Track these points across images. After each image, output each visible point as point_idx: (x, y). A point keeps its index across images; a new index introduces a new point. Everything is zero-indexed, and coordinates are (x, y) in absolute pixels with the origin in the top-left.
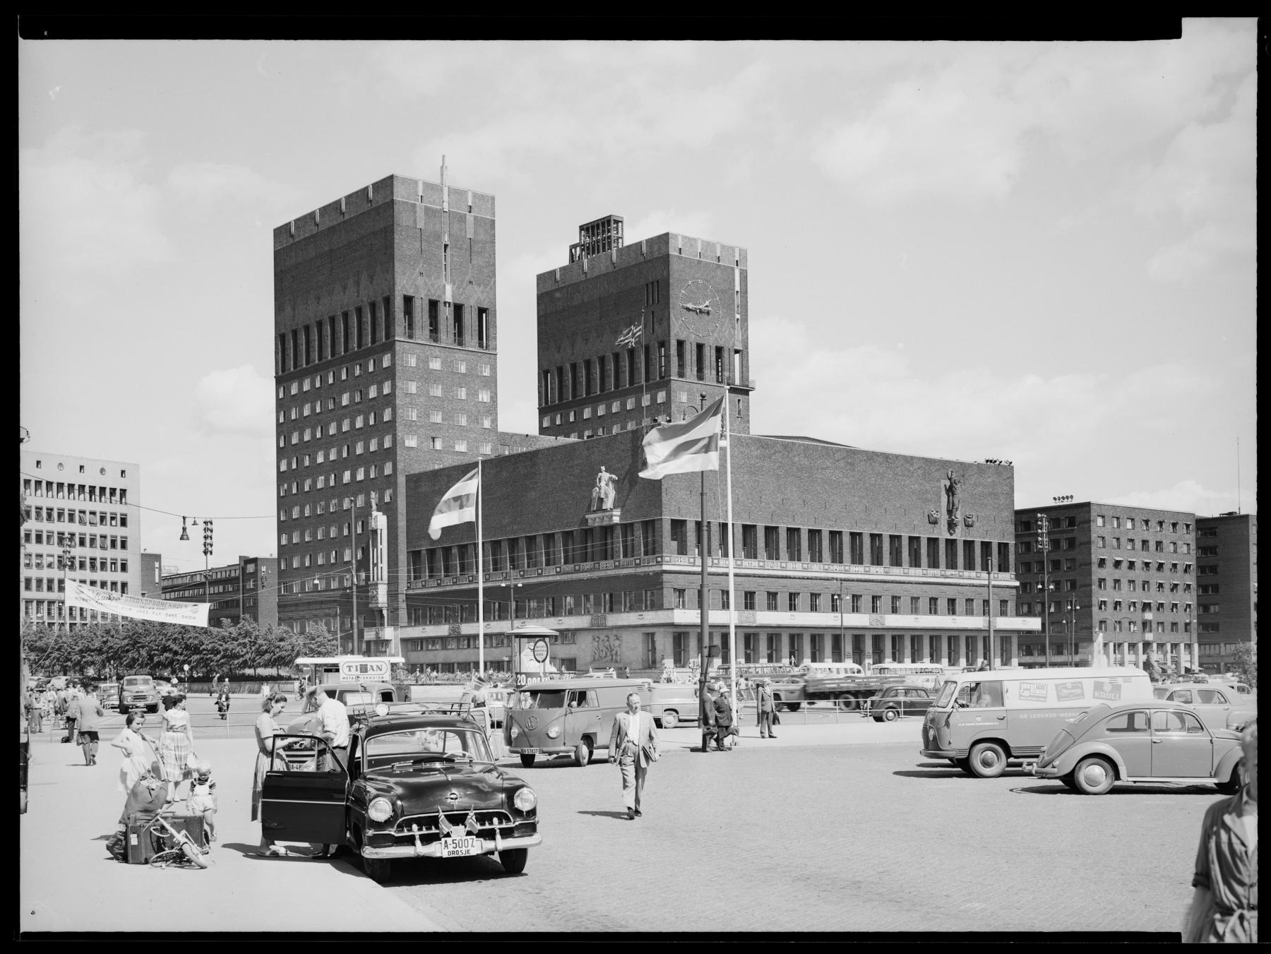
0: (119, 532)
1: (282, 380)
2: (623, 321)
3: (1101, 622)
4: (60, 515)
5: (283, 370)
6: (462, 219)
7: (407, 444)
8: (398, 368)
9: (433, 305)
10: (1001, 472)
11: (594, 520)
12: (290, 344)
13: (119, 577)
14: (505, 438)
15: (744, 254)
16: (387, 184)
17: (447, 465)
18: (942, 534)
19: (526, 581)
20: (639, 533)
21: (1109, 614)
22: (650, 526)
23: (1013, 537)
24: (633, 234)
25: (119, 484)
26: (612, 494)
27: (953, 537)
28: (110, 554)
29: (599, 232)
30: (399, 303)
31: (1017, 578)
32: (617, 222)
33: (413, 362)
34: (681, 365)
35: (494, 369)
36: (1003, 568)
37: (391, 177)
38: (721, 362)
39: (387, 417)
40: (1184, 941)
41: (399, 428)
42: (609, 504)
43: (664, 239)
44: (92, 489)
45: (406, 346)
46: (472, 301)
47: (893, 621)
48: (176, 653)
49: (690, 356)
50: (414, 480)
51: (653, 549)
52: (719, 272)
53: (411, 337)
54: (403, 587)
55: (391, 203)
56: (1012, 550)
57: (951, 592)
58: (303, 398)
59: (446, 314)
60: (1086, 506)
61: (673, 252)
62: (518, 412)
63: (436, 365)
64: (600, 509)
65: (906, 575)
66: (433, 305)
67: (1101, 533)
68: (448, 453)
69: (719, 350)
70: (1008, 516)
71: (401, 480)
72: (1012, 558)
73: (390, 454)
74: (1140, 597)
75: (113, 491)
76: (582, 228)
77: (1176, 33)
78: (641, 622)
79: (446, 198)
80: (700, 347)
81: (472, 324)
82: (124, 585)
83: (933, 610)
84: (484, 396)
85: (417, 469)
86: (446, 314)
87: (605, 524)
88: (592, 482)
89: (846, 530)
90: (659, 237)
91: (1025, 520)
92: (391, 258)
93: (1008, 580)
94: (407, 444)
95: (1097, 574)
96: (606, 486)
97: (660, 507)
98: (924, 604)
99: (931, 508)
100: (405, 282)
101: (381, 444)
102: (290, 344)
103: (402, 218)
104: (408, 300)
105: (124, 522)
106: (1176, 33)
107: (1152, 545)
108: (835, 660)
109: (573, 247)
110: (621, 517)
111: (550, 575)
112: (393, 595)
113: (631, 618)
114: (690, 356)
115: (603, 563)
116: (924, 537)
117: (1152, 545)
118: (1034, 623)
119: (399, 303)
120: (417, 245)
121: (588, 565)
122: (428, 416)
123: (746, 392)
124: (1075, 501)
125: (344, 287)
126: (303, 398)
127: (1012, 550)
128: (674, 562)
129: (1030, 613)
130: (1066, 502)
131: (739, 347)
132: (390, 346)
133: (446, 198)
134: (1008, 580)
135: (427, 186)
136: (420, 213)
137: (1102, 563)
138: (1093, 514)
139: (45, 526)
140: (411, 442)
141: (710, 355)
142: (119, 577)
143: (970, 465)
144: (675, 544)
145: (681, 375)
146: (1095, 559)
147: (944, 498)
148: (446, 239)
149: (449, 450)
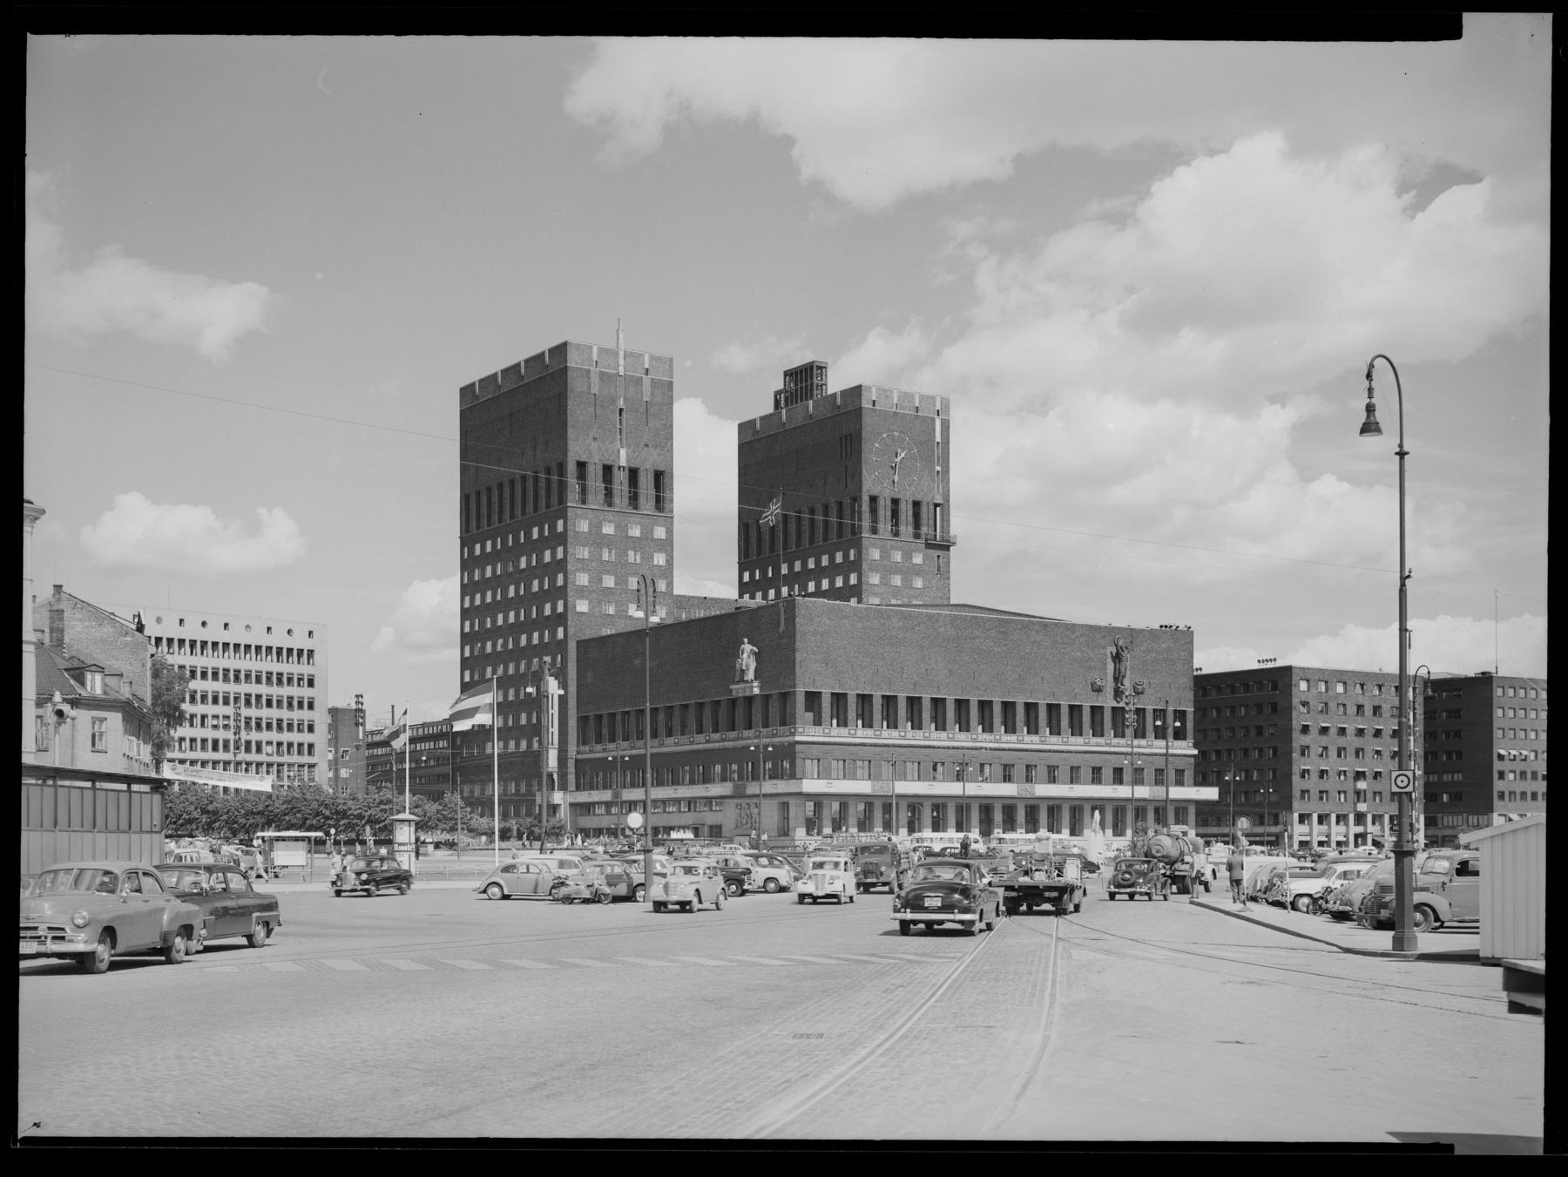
0: (306, 692)
1: (466, 542)
3: (1303, 792)
4: (248, 676)
5: (467, 531)
6: (639, 381)
7: (579, 609)
8: (570, 533)
9: (608, 470)
10: (1181, 639)
11: (737, 690)
12: (473, 506)
13: (306, 738)
14: (683, 602)
15: (946, 404)
16: (560, 350)
17: (620, 630)
18: (1108, 702)
19: (634, 752)
20: (633, 719)
21: (1313, 784)
22: (786, 697)
23: (1191, 704)
24: (836, 383)
25: (306, 645)
26: (753, 666)
28: (296, 715)
29: (803, 379)
31: (1195, 746)
33: (584, 526)
34: (875, 520)
35: (670, 532)
37: (565, 345)
38: (925, 523)
39: (560, 582)
40: (1457, 1152)
41: (570, 594)
42: (750, 675)
44: (280, 650)
45: (579, 512)
46: (647, 466)
47: (1044, 790)
48: (327, 818)
49: (884, 511)
50: (583, 645)
51: (787, 720)
52: (917, 423)
53: (584, 502)
54: (572, 750)
55: (565, 370)
57: (1096, 761)
58: (486, 558)
59: (621, 478)
61: (866, 404)
62: (707, 574)
63: (608, 529)
64: (742, 680)
65: (1066, 744)
66: (608, 470)
67: (1304, 698)
70: (1186, 682)
71: (572, 646)
73: (561, 619)
74: (1351, 764)
75: (300, 652)
77: (1455, 33)
79: (621, 362)
80: (895, 502)
81: (651, 487)
82: (311, 746)
83: (1074, 779)
84: (660, 559)
85: (589, 634)
86: (621, 478)
88: (736, 653)
89: (997, 700)
90: (853, 389)
91: (1207, 685)
92: (564, 425)
93: (1185, 748)
94: (579, 609)
95: (1299, 740)
96: (747, 658)
98: (1086, 773)
99: (1096, 677)
100: (577, 449)
101: (554, 609)
102: (473, 506)
103: (575, 385)
104: (581, 466)
105: (311, 683)
106: (1455, 33)
107: (1368, 710)
108: (1051, 830)
109: (777, 393)
110: (761, 688)
111: (700, 743)
112: (562, 760)
113: (769, 787)
114: (884, 511)
115: (746, 733)
116: (1087, 705)
117: (1368, 710)
118: (1211, 793)
119: (571, 468)
120: (591, 410)
121: (733, 734)
122: (600, 580)
123: (947, 548)
124: (1279, 664)
126: (486, 558)
128: (807, 733)
130: (1270, 665)
131: (939, 500)
132: (563, 514)
133: (621, 362)
134: (1186, 748)
136: (595, 379)
137: (1305, 729)
138: (1295, 678)
139: (199, 709)
140: (582, 606)
141: (906, 511)
142: (306, 738)
143: (1141, 631)
144: (810, 715)
145: (874, 531)
146: (1296, 724)
147: (1110, 666)
148: (621, 403)
149: (622, 614)
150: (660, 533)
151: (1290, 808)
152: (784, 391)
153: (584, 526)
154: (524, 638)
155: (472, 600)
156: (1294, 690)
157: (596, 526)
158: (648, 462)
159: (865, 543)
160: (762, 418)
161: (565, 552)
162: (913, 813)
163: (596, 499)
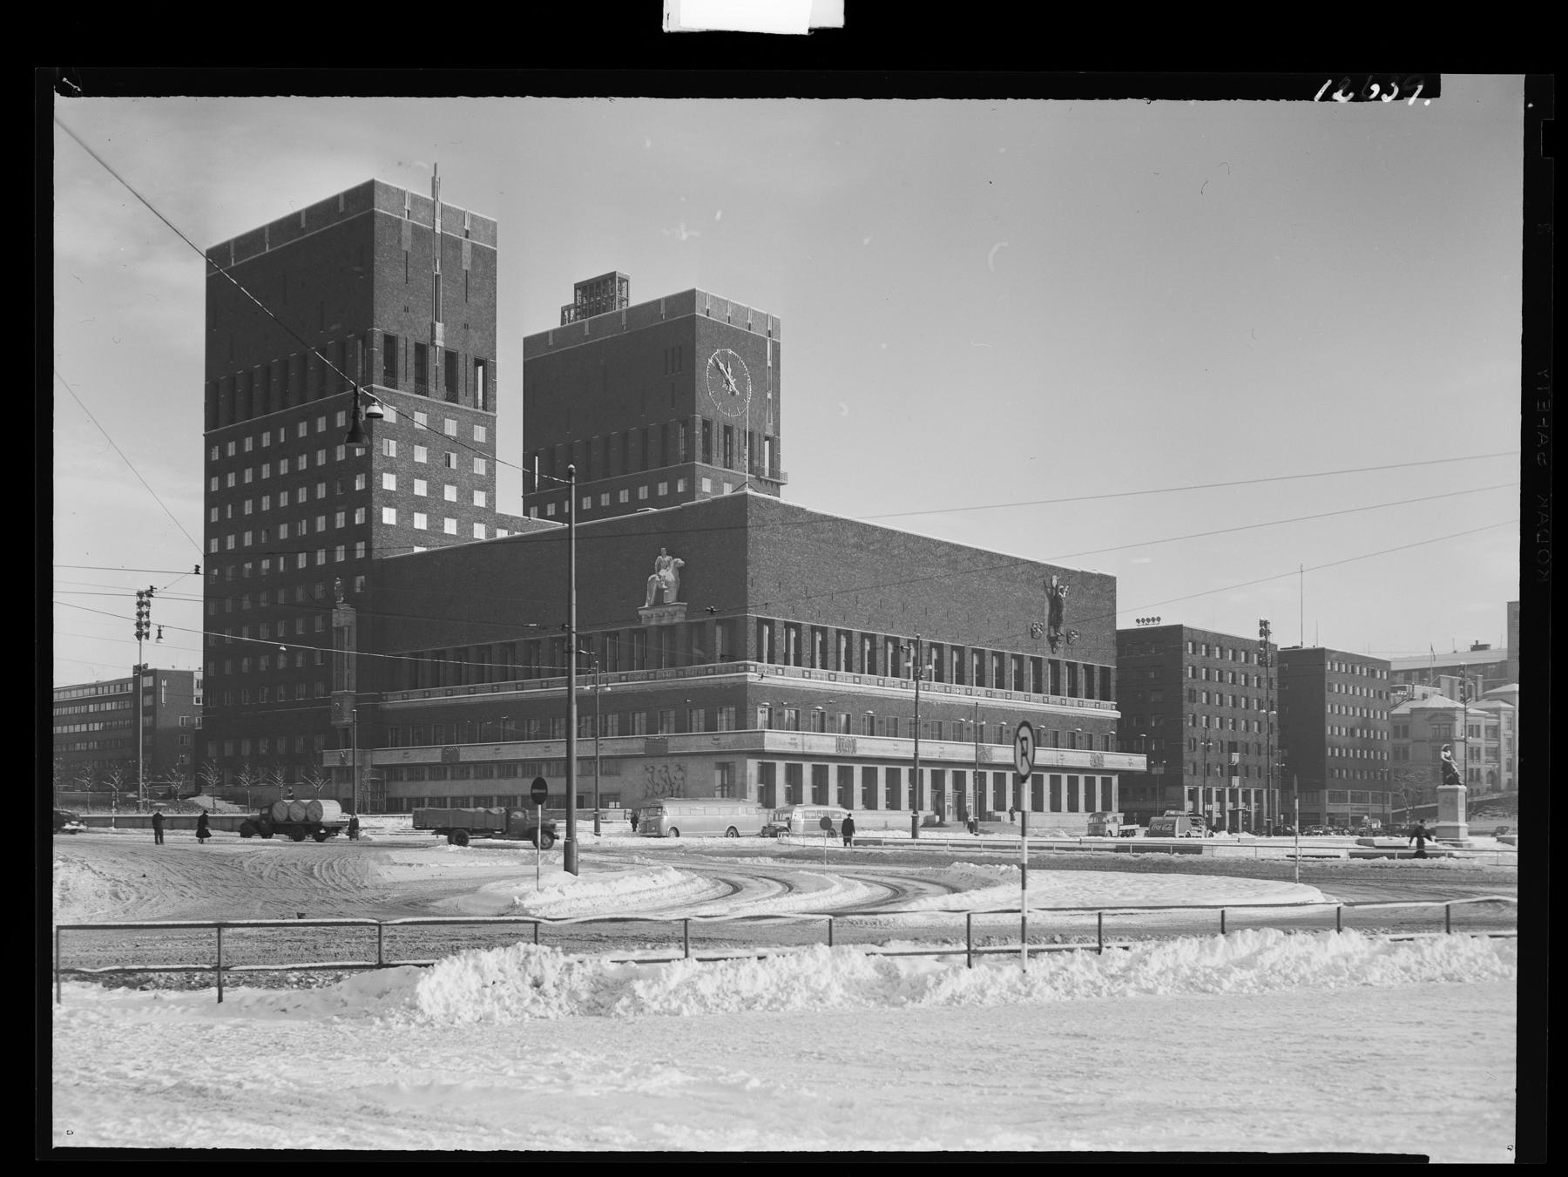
6: (457, 245)
9: (422, 351)
10: (1104, 586)
22: (734, 629)
24: (639, 295)
30: (378, 341)
32: (622, 280)
36: (1105, 697)
43: (690, 296)
56: (1113, 676)
60: (1178, 630)
68: (435, 535)
76: (578, 287)
81: (462, 376)
84: (480, 467)
87: (665, 622)
91: (1127, 639)
93: (1108, 711)
97: (745, 599)
100: (385, 322)
101: (350, 519)
109: (568, 308)
118: (1138, 762)
119: (378, 341)
120: (402, 271)
124: (1162, 624)
125: (302, 331)
127: (1113, 676)
130: (1151, 625)
131: (770, 433)
135: (416, 200)
136: (407, 233)
140: (389, 516)
145: (708, 460)
150: (480, 434)
151: (1180, 783)
152: (575, 306)
153: (390, 415)
155: (222, 544)
158: (468, 350)
159: (698, 472)
163: (406, 390)
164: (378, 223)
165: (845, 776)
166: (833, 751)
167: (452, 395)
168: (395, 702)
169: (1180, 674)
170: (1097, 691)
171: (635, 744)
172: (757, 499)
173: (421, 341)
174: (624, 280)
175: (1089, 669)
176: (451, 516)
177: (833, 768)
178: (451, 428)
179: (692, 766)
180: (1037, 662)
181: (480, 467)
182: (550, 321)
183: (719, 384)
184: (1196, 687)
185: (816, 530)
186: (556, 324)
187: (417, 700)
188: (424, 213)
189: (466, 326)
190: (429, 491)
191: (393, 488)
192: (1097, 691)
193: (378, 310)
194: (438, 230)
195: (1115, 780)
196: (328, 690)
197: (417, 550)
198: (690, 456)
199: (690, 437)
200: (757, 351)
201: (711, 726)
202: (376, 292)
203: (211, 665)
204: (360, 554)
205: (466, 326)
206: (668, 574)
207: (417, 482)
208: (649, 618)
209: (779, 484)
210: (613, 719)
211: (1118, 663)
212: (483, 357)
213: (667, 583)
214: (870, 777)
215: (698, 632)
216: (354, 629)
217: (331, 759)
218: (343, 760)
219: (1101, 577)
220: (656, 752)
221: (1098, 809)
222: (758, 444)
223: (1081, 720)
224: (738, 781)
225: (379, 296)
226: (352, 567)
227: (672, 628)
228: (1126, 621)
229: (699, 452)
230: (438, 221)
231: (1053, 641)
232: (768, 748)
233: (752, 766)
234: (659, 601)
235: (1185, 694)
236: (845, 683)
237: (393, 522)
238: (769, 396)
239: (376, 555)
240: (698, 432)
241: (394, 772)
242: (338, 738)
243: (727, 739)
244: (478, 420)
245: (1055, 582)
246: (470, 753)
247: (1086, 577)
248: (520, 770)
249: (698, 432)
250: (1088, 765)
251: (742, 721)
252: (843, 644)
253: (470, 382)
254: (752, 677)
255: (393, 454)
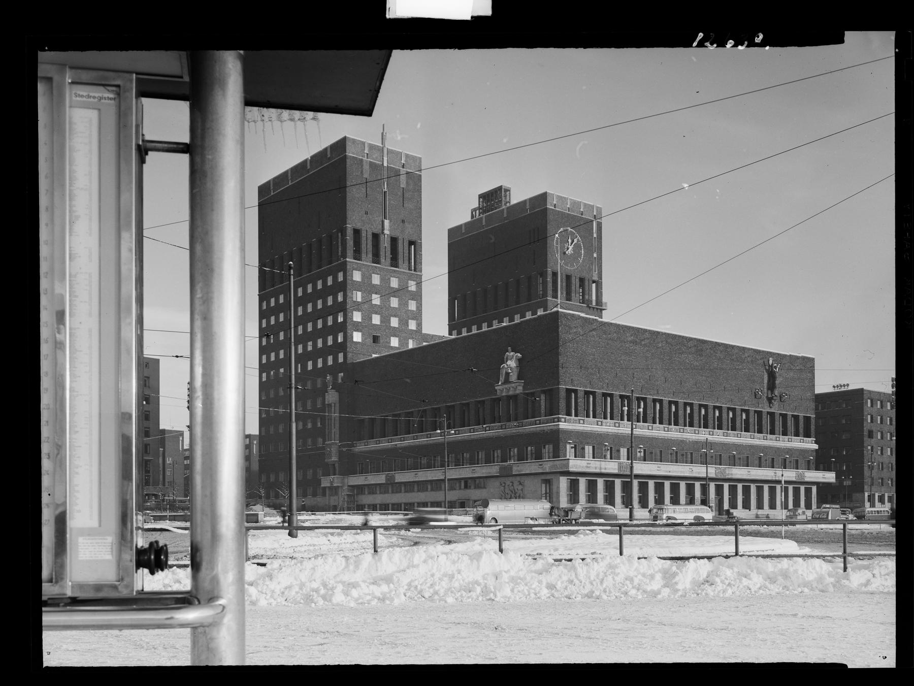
2: (515, 255)
7: (355, 340)
8: (349, 282)
9: (376, 237)
10: (807, 365)
11: (501, 389)
14: (426, 337)
22: (552, 395)
24: (516, 197)
27: (772, 410)
36: (807, 435)
43: (543, 197)
56: (813, 421)
59: (385, 244)
60: (860, 392)
62: (435, 321)
69: (582, 280)
72: (813, 427)
76: (481, 196)
78: (541, 471)
81: (402, 252)
84: (412, 305)
87: (511, 393)
91: (822, 399)
93: (810, 445)
94: (355, 340)
109: (474, 210)
118: (829, 477)
120: (364, 190)
124: (850, 388)
127: (813, 421)
129: (829, 469)
130: (843, 389)
131: (595, 278)
135: (372, 147)
136: (366, 167)
141: (575, 282)
150: (412, 286)
152: (479, 208)
154: (310, 364)
155: (268, 358)
156: (865, 407)
157: (367, 278)
160: (466, 224)
161: (345, 296)
162: (58, 450)
163: (367, 261)
164: (348, 161)
165: (627, 487)
166: (616, 471)
167: (394, 262)
168: (360, 447)
169: (862, 421)
170: (801, 431)
171: (494, 469)
172: (565, 314)
173: (375, 231)
174: (507, 190)
175: (796, 418)
176: (395, 336)
177: (618, 483)
178: (376, 280)
179: (528, 482)
180: (759, 414)
181: (412, 305)
182: (465, 218)
183: (563, 252)
184: (874, 429)
185: (605, 333)
186: (468, 219)
187: (373, 445)
188: (376, 155)
189: (403, 221)
190: (381, 322)
191: (360, 320)
192: (801, 431)
193: (349, 214)
194: (385, 165)
195: (814, 489)
196: (324, 441)
197: (374, 356)
198: (545, 294)
199: (545, 283)
200: (587, 226)
201: (538, 456)
202: (348, 203)
203: (263, 429)
204: (341, 360)
205: (403, 221)
206: (512, 363)
207: (374, 316)
208: (502, 391)
209: (602, 310)
210: (482, 455)
211: (816, 414)
212: (413, 239)
213: (511, 369)
214: (643, 488)
215: (529, 397)
216: (338, 405)
217: (325, 482)
218: (332, 483)
219: (804, 358)
220: (506, 473)
221: (791, 506)
222: (585, 286)
223: (790, 451)
224: (555, 490)
225: (349, 205)
226: (337, 368)
227: (515, 397)
228: (823, 386)
229: (550, 292)
230: (385, 159)
231: (770, 400)
232: (571, 469)
233: (564, 482)
234: (507, 381)
235: (866, 433)
236: (718, 436)
237: (360, 340)
238: (595, 255)
239: (349, 362)
240: (549, 279)
241: (360, 489)
242: (329, 470)
243: (548, 466)
244: (411, 278)
245: (771, 362)
246: (402, 477)
247: (793, 359)
248: (429, 487)
249: (549, 279)
250: (794, 479)
251: (557, 453)
252: (688, 411)
253: (406, 255)
254: (563, 425)
255: (359, 300)
